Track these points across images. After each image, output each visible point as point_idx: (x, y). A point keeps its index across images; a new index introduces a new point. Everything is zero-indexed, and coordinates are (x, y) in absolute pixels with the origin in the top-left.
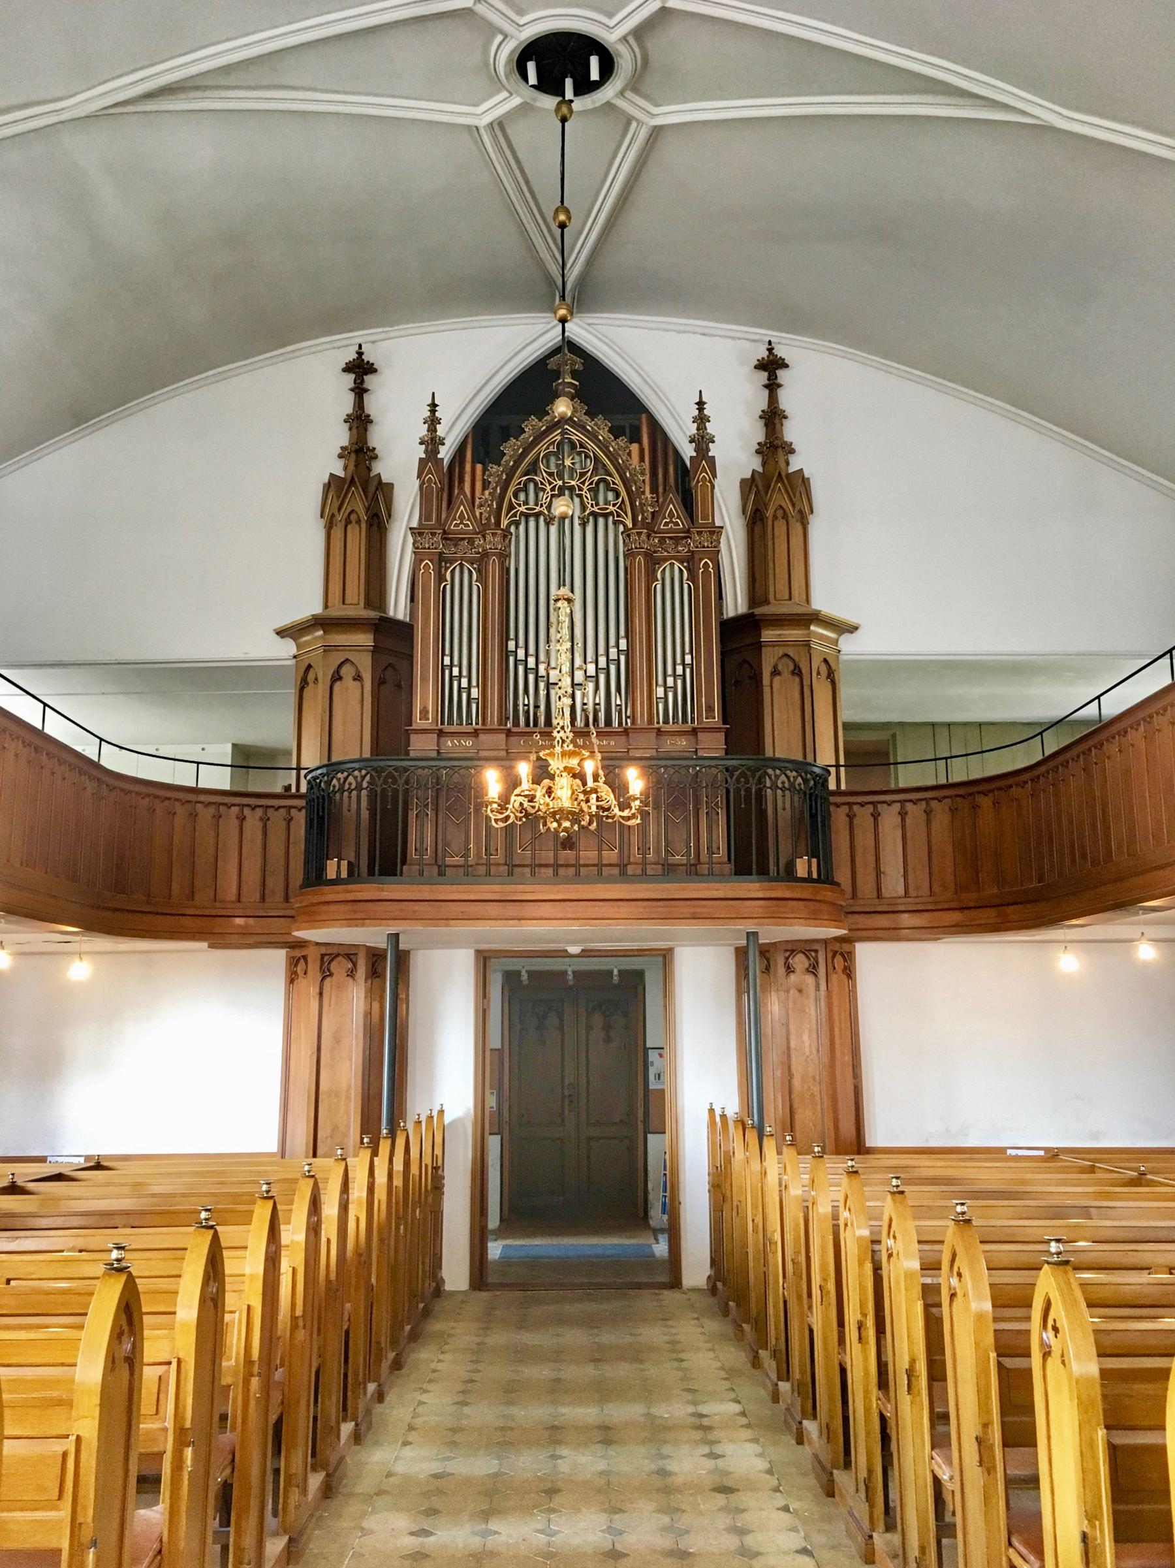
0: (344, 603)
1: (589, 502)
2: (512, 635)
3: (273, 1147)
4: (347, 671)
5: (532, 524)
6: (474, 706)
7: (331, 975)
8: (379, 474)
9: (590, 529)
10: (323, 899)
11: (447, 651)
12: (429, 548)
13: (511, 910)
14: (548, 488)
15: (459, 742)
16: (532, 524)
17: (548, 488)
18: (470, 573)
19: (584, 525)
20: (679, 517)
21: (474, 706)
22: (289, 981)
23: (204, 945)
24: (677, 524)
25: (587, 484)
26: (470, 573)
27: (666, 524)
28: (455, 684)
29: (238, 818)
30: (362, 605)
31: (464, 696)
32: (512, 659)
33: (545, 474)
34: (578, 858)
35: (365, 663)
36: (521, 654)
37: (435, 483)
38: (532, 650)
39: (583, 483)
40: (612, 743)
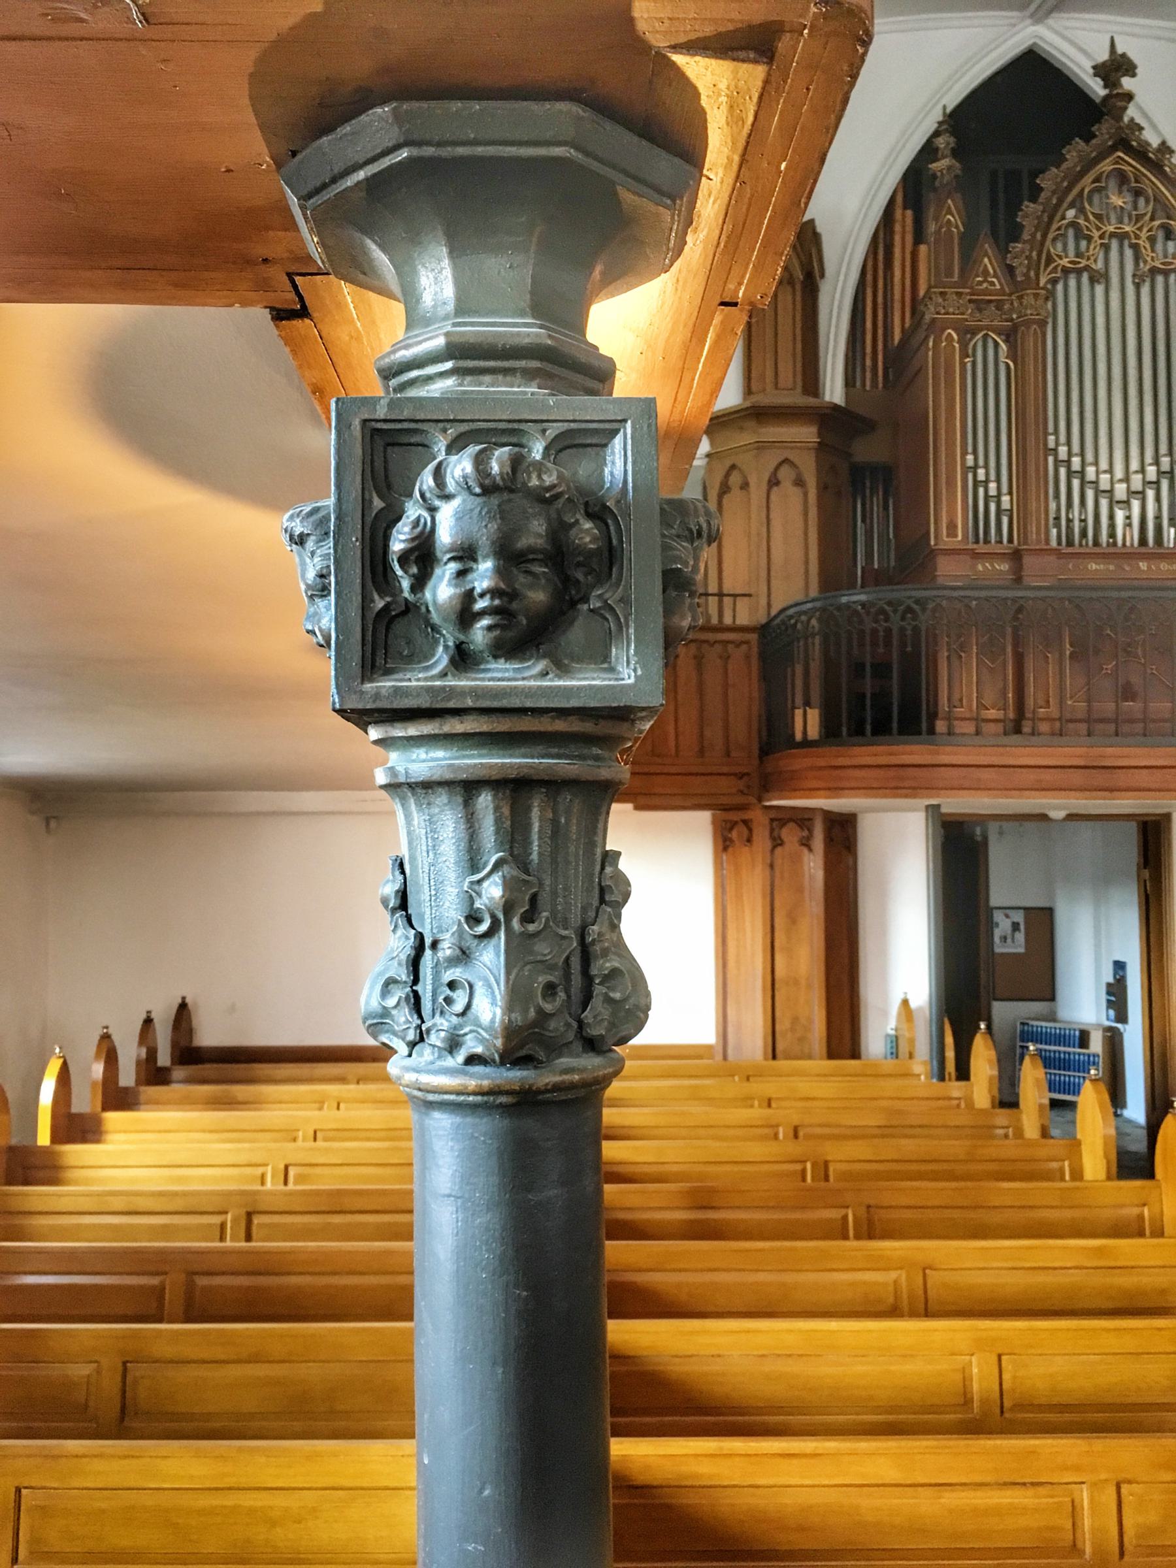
0: (777, 388)
1: (1146, 252)
2: (1051, 429)
3: (707, 1035)
4: (785, 474)
5: (1072, 283)
6: (1005, 520)
7: (781, 844)
8: (812, 221)
9: (1145, 290)
10: (856, 761)
11: (970, 449)
12: (954, 314)
13: (1100, 778)
14: (1096, 234)
15: (992, 566)
16: (1072, 283)
17: (1096, 234)
18: (996, 345)
19: (1138, 287)
20: (995, 276)
21: (1005, 520)
22: (721, 847)
23: (630, 806)
24: (992, 284)
25: (1145, 230)
26: (996, 345)
27: (980, 283)
28: (981, 491)
29: (721, 657)
30: (799, 389)
31: (993, 507)
32: (1051, 459)
33: (1091, 217)
34: (1145, 711)
35: (808, 466)
36: (1063, 451)
37: (957, 227)
38: (1076, 448)
39: (1140, 229)
40: (1112, 567)
